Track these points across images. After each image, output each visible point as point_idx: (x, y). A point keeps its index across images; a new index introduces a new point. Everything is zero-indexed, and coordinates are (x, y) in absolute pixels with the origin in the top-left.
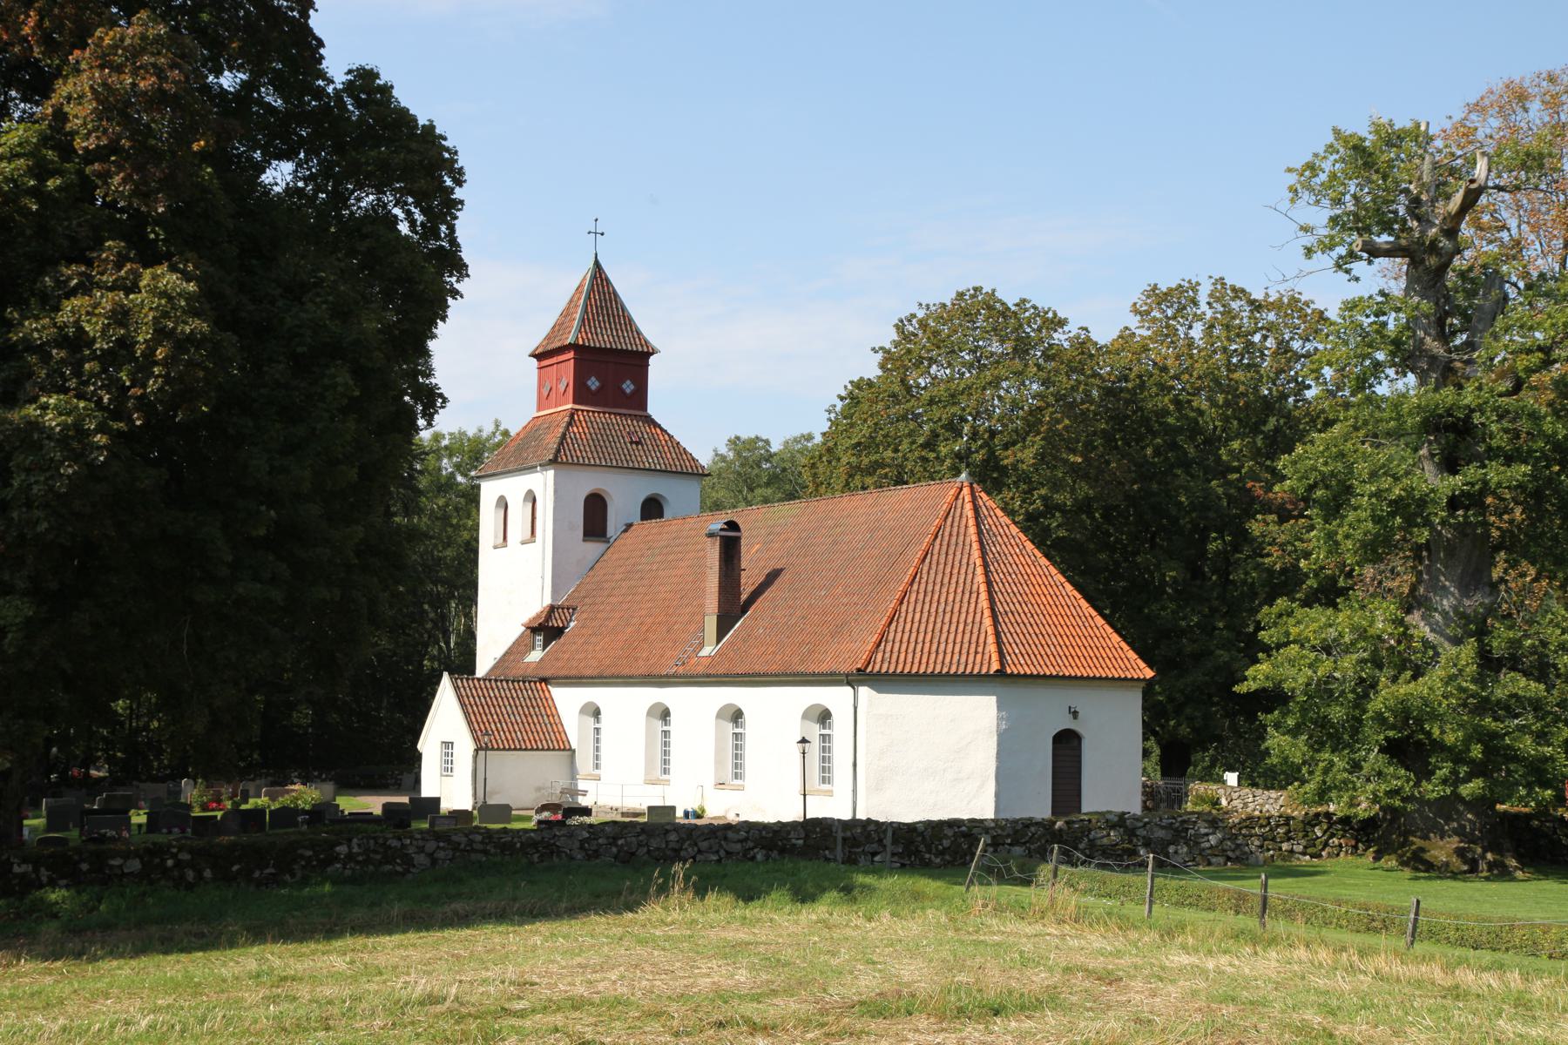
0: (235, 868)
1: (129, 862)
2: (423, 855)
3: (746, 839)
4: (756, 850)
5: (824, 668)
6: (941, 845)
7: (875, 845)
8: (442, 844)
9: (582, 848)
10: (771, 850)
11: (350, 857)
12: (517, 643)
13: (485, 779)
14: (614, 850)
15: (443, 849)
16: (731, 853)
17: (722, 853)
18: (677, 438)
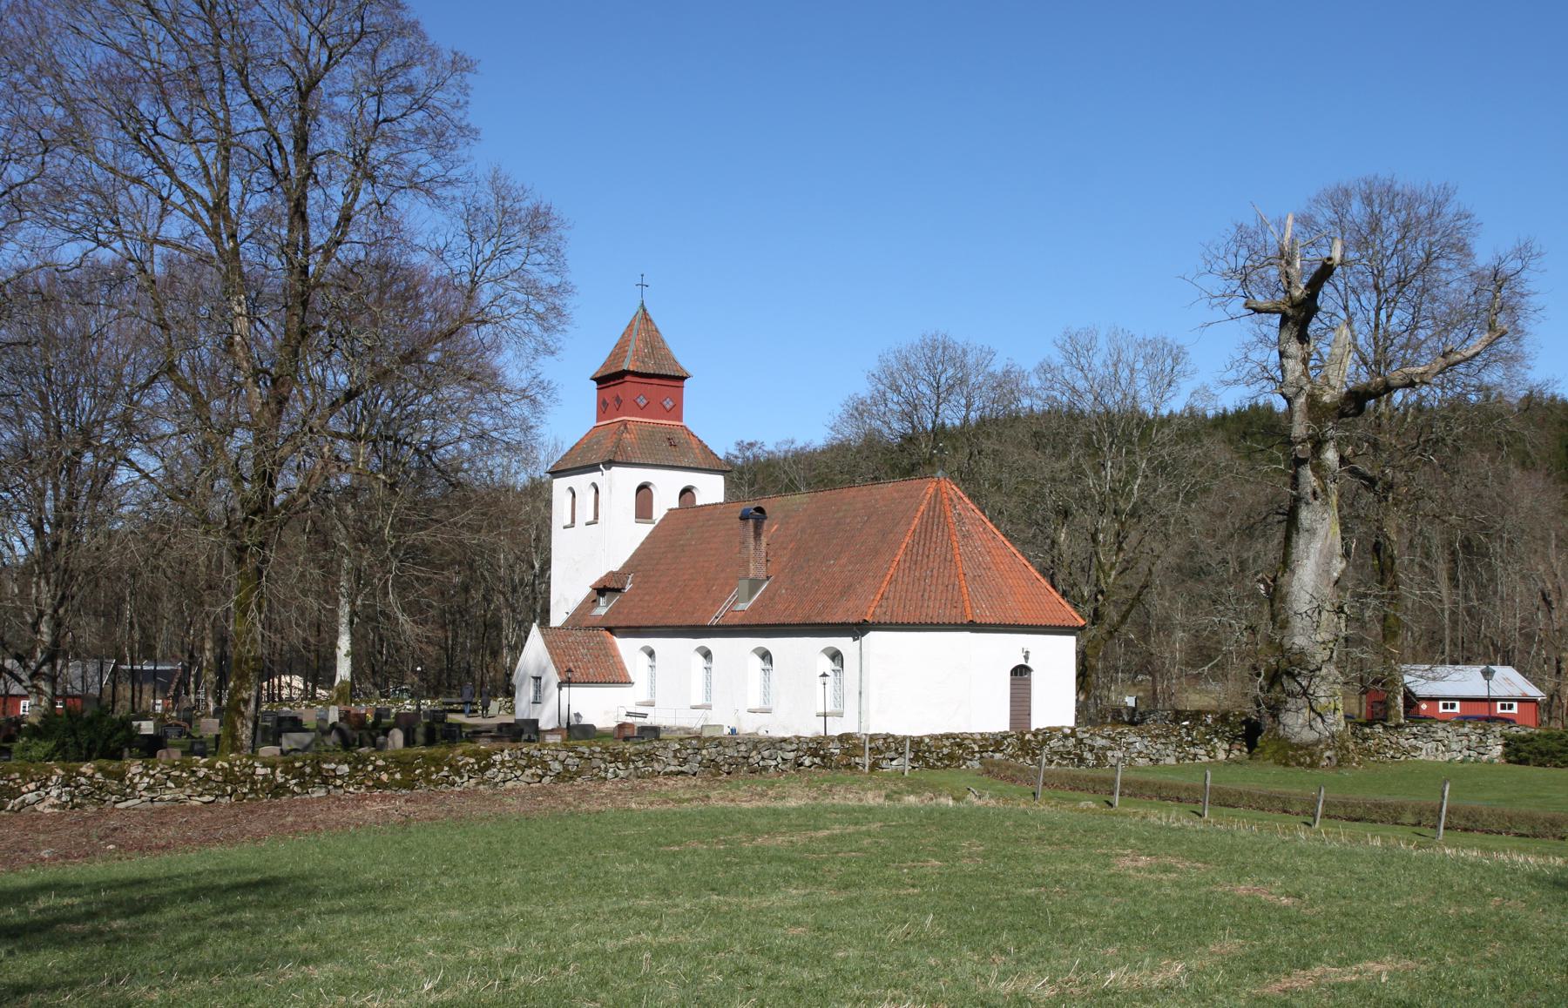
0: (417, 772)
1: (340, 767)
3: (797, 750)
9: (675, 756)
11: (502, 763)
12: (585, 602)
14: (699, 758)
17: (779, 759)
18: (706, 442)
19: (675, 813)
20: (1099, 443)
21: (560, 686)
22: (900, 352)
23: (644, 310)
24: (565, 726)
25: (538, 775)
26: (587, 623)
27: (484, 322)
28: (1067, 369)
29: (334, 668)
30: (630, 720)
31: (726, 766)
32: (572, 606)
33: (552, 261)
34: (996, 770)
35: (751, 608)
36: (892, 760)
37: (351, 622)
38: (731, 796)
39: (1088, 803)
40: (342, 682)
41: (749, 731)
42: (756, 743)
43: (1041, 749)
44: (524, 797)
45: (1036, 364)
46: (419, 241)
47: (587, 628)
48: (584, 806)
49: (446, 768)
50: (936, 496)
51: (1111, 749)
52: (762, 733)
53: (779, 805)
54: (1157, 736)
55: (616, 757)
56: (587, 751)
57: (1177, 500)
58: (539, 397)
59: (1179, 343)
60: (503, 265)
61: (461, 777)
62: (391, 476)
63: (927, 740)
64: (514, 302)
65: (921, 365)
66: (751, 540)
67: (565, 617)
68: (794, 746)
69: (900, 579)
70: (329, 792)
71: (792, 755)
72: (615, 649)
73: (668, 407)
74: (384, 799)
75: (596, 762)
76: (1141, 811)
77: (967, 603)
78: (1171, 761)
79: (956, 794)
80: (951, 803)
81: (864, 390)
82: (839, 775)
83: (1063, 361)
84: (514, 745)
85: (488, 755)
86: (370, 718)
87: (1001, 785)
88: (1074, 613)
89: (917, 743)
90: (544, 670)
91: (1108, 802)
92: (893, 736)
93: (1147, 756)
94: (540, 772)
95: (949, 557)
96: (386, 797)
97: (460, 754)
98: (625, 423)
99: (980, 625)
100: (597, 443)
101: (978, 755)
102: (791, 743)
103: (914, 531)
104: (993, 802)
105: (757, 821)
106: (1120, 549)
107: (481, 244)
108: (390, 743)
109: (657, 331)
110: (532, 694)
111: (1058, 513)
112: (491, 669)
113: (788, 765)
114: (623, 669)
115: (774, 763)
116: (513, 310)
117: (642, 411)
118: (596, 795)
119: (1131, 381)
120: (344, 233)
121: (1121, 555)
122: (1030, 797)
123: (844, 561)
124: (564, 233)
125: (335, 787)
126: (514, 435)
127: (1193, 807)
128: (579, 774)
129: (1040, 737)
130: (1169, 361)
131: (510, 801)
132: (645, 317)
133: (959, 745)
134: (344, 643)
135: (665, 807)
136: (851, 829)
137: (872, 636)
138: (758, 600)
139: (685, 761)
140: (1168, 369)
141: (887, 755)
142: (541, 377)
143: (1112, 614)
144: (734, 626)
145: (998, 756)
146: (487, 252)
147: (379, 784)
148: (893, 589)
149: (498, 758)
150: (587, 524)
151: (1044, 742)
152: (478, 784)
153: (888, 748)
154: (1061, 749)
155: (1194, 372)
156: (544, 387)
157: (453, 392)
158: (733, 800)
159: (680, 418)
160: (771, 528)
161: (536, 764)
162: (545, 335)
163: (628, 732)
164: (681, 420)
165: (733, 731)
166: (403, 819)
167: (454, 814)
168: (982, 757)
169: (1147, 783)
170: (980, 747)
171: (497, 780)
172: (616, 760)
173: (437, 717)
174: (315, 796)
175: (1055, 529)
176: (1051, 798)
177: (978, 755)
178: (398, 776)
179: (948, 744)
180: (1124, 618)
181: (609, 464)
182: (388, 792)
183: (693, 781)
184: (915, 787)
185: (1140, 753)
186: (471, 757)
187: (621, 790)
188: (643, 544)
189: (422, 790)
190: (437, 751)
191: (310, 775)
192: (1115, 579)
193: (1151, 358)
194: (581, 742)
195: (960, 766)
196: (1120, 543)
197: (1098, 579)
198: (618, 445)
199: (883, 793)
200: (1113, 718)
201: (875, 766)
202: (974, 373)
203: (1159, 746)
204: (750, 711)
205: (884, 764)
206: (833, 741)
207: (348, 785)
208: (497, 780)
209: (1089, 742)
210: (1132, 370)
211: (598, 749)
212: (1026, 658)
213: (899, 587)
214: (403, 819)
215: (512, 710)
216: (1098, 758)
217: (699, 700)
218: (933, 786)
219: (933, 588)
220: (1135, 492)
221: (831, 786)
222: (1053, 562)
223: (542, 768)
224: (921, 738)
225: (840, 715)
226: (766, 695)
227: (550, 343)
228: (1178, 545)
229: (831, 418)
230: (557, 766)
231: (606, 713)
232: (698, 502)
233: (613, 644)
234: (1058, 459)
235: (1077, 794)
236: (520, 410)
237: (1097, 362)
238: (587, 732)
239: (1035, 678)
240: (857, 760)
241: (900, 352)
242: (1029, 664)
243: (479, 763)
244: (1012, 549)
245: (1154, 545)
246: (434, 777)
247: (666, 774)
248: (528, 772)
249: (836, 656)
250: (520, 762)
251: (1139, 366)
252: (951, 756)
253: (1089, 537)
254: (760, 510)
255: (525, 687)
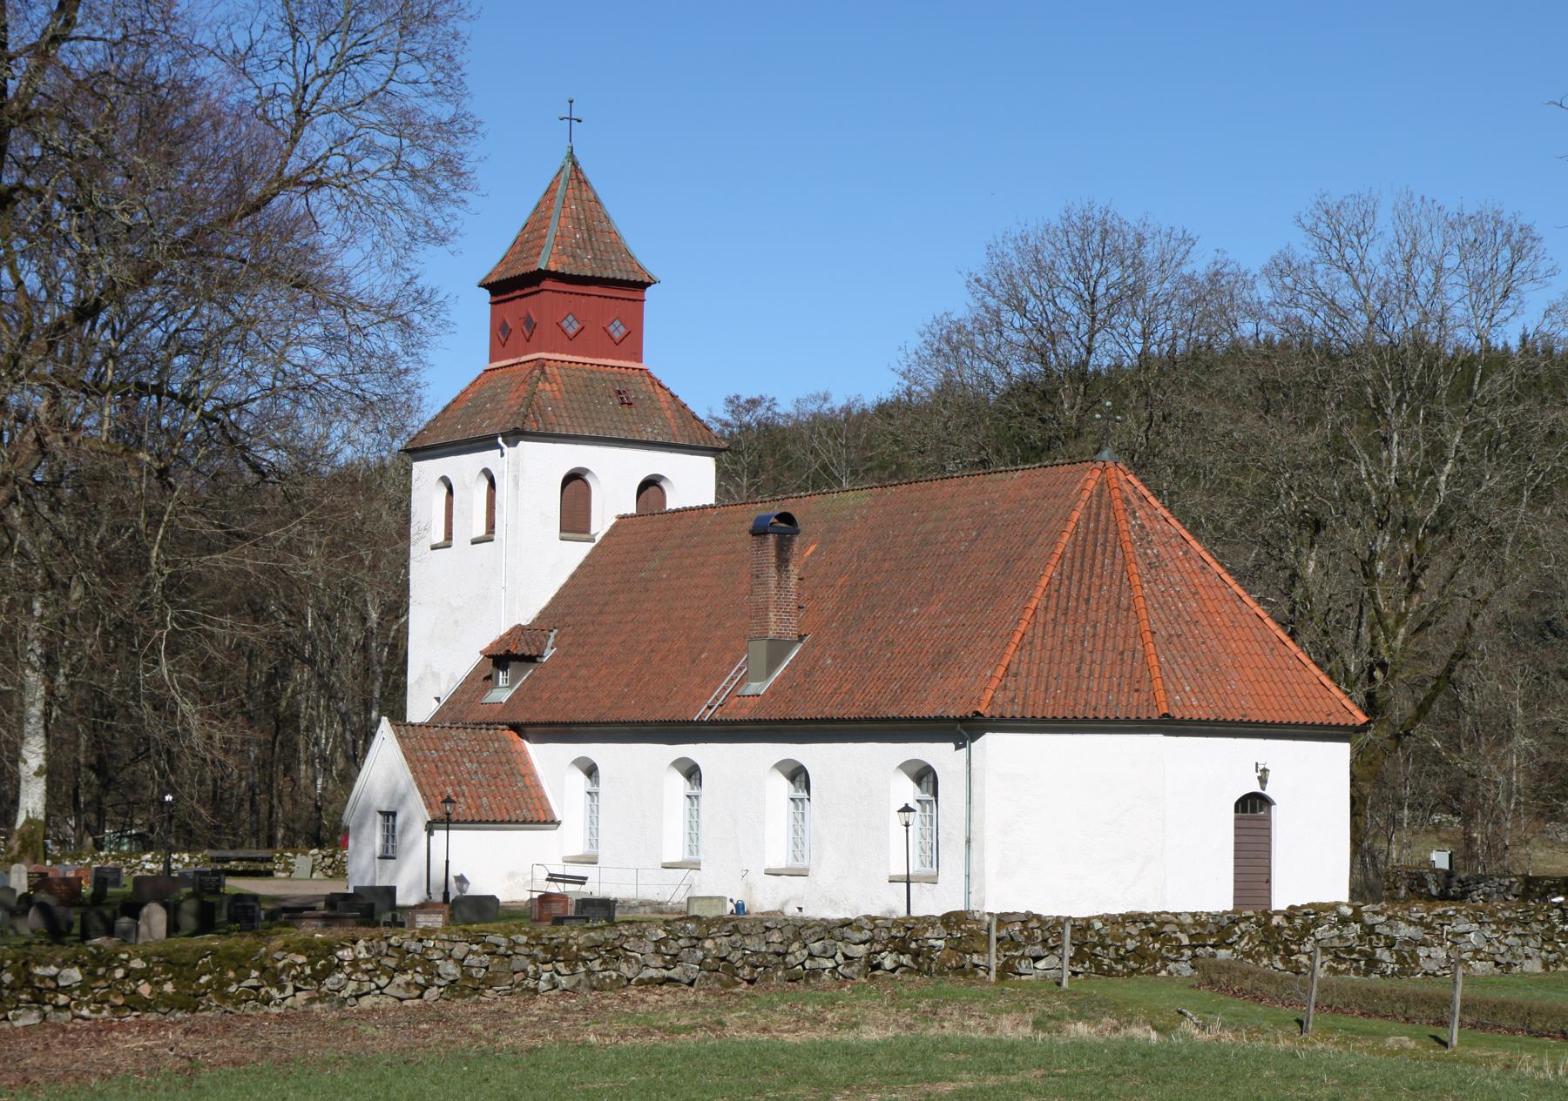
0: (204, 979)
1: (65, 972)
2: (451, 962)
3: (871, 941)
4: (883, 954)
5: (926, 711)
6: (1124, 946)
7: (1038, 947)
8: (475, 947)
9: (657, 952)
10: (903, 954)
11: (355, 963)
12: (470, 679)
13: (447, 862)
14: (700, 954)
15: (475, 953)
16: (852, 958)
17: (839, 958)
18: (683, 398)
19: (670, 1052)
20: (1377, 400)
21: (430, 828)
22: (1025, 239)
23: (575, 164)
24: (438, 898)
25: (417, 985)
26: (475, 716)
27: (318, 184)
28: (1320, 268)
29: (15, 802)
30: (554, 888)
31: (747, 970)
32: (446, 686)
33: (440, 76)
34: (1224, 979)
35: (772, 692)
36: (1037, 959)
37: (47, 715)
38: (761, 1022)
39: (1401, 1040)
40: (29, 821)
41: (767, 908)
42: (800, 929)
43: (1300, 942)
44: (395, 1023)
45: (1265, 260)
46: (204, 37)
47: (477, 725)
48: (505, 1040)
49: (255, 974)
50: (1100, 495)
51: (1424, 943)
52: (791, 911)
53: (848, 1036)
54: (1508, 922)
55: (555, 952)
56: (503, 941)
57: (1517, 501)
58: (416, 318)
59: (1524, 220)
60: (350, 83)
61: (282, 989)
62: (159, 457)
63: (1098, 925)
64: (370, 149)
65: (1063, 263)
66: (772, 571)
67: (434, 706)
68: (866, 935)
69: (1038, 641)
70: (44, 1017)
71: (861, 950)
72: (527, 763)
73: (617, 335)
74: (145, 1028)
75: (519, 962)
76: (1502, 1055)
77: (1158, 684)
78: (1535, 966)
79: (1159, 1021)
80: (1154, 1035)
81: (961, 306)
82: (946, 985)
83: (1314, 254)
84: (373, 932)
85: (330, 949)
86: (87, 889)
87: (1237, 1006)
88: (1346, 702)
89: (1082, 927)
90: (403, 799)
91: (1436, 1039)
92: (1038, 917)
93: (1491, 957)
94: (420, 979)
95: (1124, 601)
96: (148, 1024)
97: (280, 949)
98: (541, 364)
99: (1182, 721)
100: (492, 399)
101: (1188, 953)
102: (861, 929)
103: (1062, 557)
104: (1228, 1037)
105: (821, 1065)
106: (1413, 588)
107: (313, 44)
108: (143, 929)
109: (597, 201)
110: (378, 841)
111: (1302, 524)
112: (286, 799)
113: (855, 968)
114: (542, 798)
115: (830, 964)
116: (370, 164)
117: (571, 342)
118: (523, 1020)
119: (1437, 288)
120: (69, 23)
121: (1416, 599)
122: (1295, 1028)
123: (936, 608)
124: (462, 26)
125: (57, 1007)
126: (373, 387)
127: (1433, 1030)
128: (489, 982)
129: (1298, 921)
130: (1506, 253)
131: (371, 1030)
132: (575, 174)
133: (1155, 935)
134: (34, 755)
135: (648, 1041)
136: (992, 1081)
137: (991, 743)
138: (783, 677)
139: (676, 959)
140: (1503, 268)
141: (1029, 951)
142: (420, 283)
143: (1402, 706)
144: (742, 722)
145: (1223, 953)
146: (324, 60)
147: (135, 1003)
148: (1025, 658)
149: (346, 954)
150: (434, 548)
151: (1306, 930)
152: (311, 1001)
153: (1030, 939)
154: (1336, 943)
155: (1552, 272)
156: (421, 299)
157: (269, 302)
158: (765, 1030)
159: (638, 357)
160: (805, 550)
161: (413, 966)
162: (430, 208)
163: (557, 910)
164: (640, 360)
165: (740, 907)
166: (186, 1063)
167: (275, 1054)
168: (1195, 956)
169: (1504, 1005)
170: (1191, 937)
171: (344, 994)
172: (554, 959)
173: (206, 885)
174: (19, 1024)
175: (1297, 554)
176: (1333, 1029)
177: (1188, 953)
178: (169, 988)
179: (1135, 931)
180: (1422, 710)
181: (515, 435)
182: (152, 1017)
183: (691, 995)
184: (1085, 1009)
185: (1477, 951)
186: (299, 952)
187: (566, 1010)
188: (573, 577)
189: (211, 1013)
190: (238, 942)
191: (11, 987)
192: (1405, 641)
193: (1470, 249)
194: (491, 927)
195: (1156, 972)
196: (1415, 578)
197: (1374, 643)
198: (530, 401)
199: (1029, 1017)
200: (1410, 889)
201: (1007, 970)
202: (1158, 276)
203: (1511, 940)
204: (769, 873)
205: (1023, 966)
206: (933, 925)
207: (79, 1005)
208: (344, 994)
209: (1386, 930)
210: (1439, 269)
211: (523, 939)
212: (1263, 781)
213: (1036, 654)
214: (186, 1063)
215: (339, 871)
216: (1401, 959)
217: (677, 854)
218: (1116, 1006)
219: (1097, 656)
220: (1442, 486)
221: (935, 1005)
222: (1292, 611)
223: (425, 972)
224: (1088, 920)
225: (933, 880)
226: (798, 842)
227: (438, 223)
228: (1519, 585)
229: (901, 355)
230: (450, 969)
231: (511, 875)
232: (672, 503)
233: (524, 753)
234: (1300, 430)
235: (1374, 1024)
236: (387, 340)
237: (1374, 255)
238: (485, 907)
239: (1280, 818)
240: (976, 959)
241: (1025, 239)
242: (1267, 792)
243: (312, 964)
244: (1237, 588)
245: (1477, 582)
246: (232, 989)
247: (641, 982)
248: (400, 979)
249: (924, 776)
250: (386, 961)
251: (1451, 262)
252: (1140, 954)
253: (1357, 567)
254: (786, 518)
255: (366, 831)
